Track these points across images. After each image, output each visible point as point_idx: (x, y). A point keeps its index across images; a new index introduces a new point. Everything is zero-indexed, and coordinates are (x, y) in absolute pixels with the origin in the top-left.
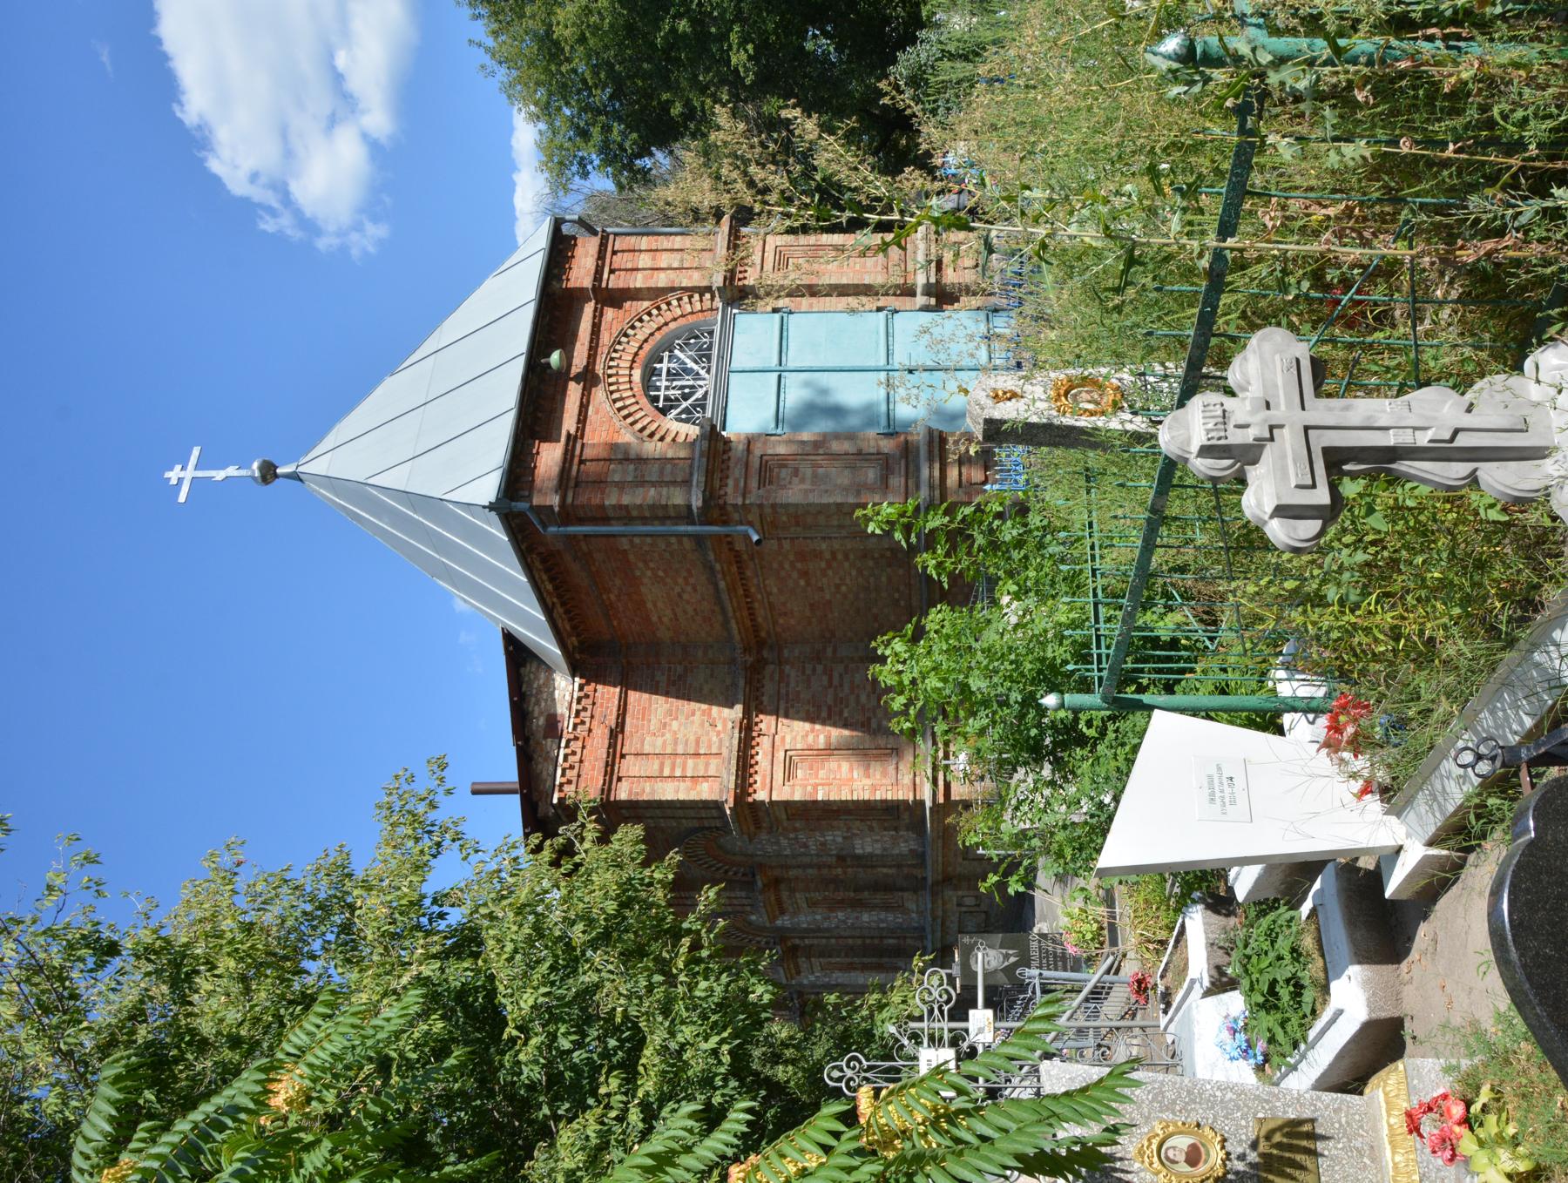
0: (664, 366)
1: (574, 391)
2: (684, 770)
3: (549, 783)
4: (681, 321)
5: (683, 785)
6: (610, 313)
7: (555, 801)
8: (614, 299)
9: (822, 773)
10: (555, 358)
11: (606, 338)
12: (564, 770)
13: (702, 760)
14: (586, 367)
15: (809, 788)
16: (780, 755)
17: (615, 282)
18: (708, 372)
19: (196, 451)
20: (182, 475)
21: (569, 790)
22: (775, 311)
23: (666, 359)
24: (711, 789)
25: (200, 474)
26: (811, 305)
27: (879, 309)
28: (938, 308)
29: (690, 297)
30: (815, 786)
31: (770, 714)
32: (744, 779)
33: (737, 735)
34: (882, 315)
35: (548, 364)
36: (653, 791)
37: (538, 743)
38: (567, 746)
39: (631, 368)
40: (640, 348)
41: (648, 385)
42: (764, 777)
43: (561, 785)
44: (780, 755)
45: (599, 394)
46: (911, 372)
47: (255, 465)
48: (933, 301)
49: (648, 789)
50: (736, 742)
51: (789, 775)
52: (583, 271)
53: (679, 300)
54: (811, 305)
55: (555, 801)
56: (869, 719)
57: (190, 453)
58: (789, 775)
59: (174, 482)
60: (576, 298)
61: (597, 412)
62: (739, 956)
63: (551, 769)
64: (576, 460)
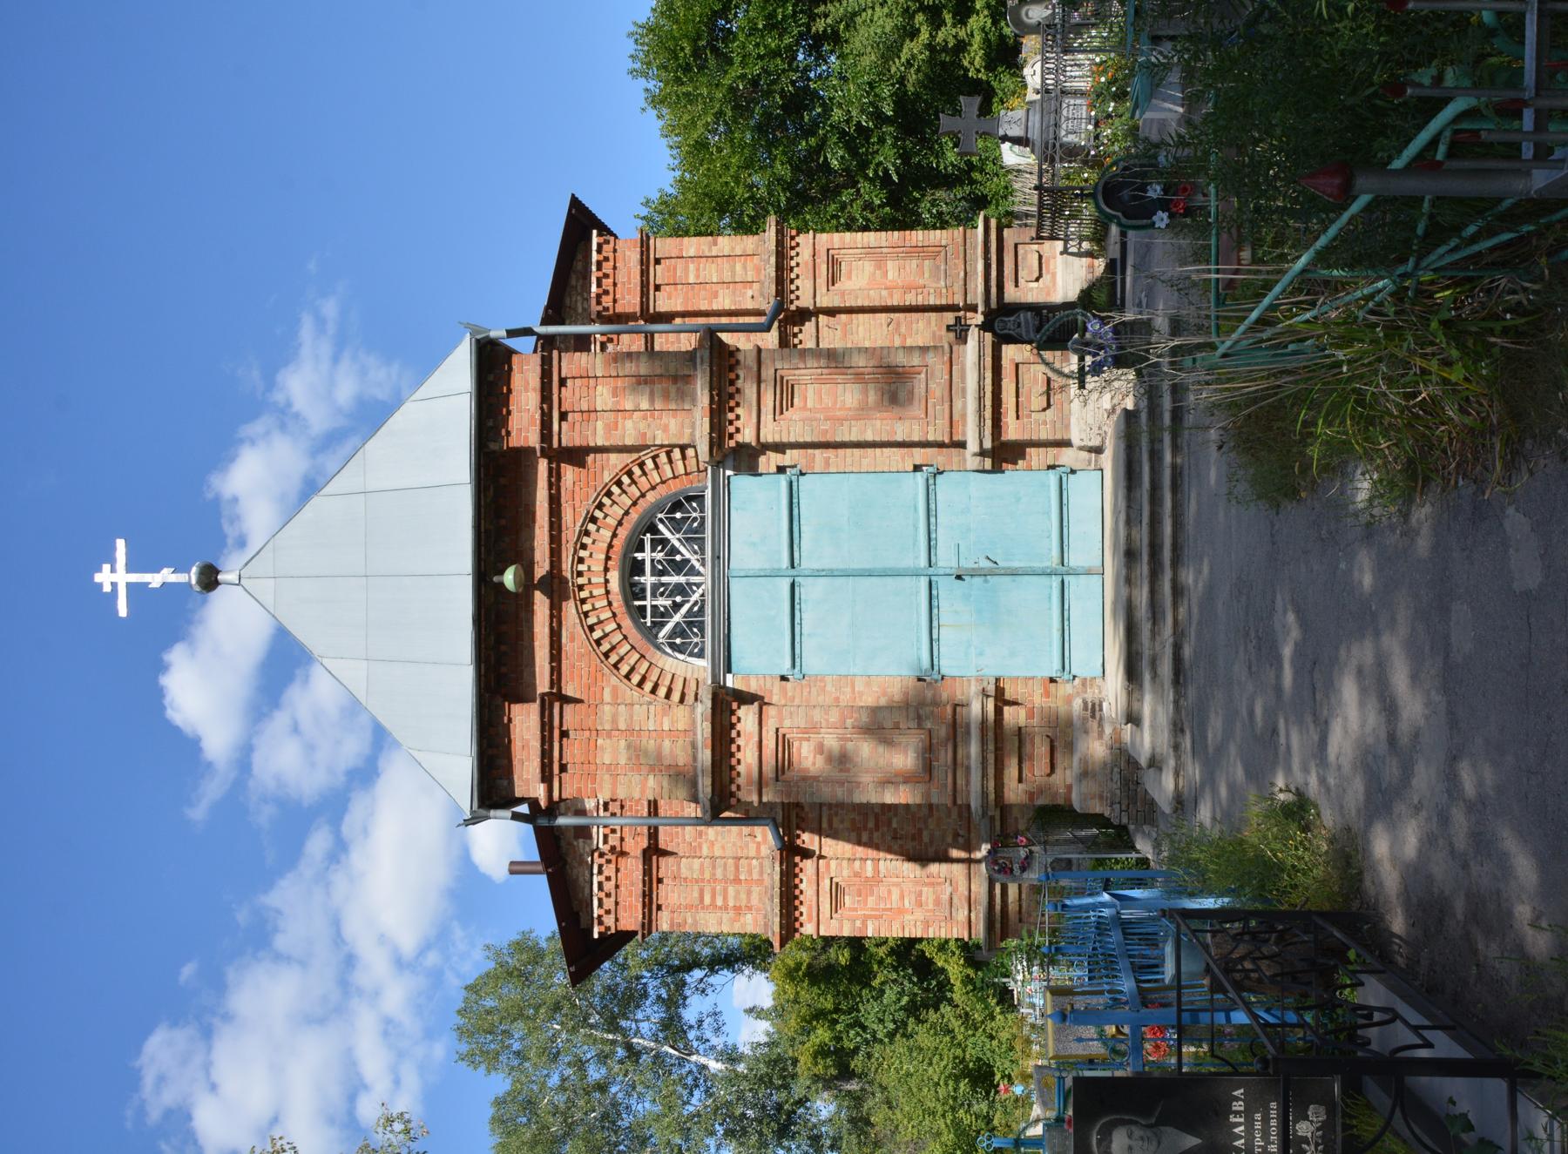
0: (646, 556)
1: (541, 603)
2: (725, 898)
3: (587, 891)
4: (662, 490)
5: (725, 917)
6: (569, 473)
7: (596, 936)
8: (577, 456)
9: (871, 901)
10: (509, 578)
11: (571, 520)
12: (600, 900)
13: (743, 888)
14: (550, 573)
15: (858, 923)
16: (825, 884)
17: (569, 435)
18: (703, 565)
19: (123, 611)
20: (114, 577)
21: (609, 921)
22: (781, 470)
23: (648, 546)
24: (755, 920)
25: (135, 578)
26: (827, 462)
27: (917, 468)
28: (997, 469)
29: (668, 454)
30: (865, 919)
31: (812, 831)
32: (788, 882)
33: (778, 869)
34: (920, 478)
35: (502, 584)
36: (695, 922)
37: (570, 844)
38: (600, 872)
39: (606, 570)
40: (614, 535)
41: (633, 592)
42: (810, 907)
43: (600, 917)
44: (825, 884)
45: (570, 609)
46: (959, 577)
47: (194, 569)
48: (988, 463)
49: (690, 921)
50: (777, 877)
51: (836, 904)
52: (525, 422)
53: (654, 458)
54: (827, 462)
55: (596, 936)
56: (920, 830)
57: (114, 549)
58: (836, 904)
59: (107, 588)
60: (523, 457)
61: (572, 640)
62: (840, 194)
63: (587, 873)
64: (556, 733)
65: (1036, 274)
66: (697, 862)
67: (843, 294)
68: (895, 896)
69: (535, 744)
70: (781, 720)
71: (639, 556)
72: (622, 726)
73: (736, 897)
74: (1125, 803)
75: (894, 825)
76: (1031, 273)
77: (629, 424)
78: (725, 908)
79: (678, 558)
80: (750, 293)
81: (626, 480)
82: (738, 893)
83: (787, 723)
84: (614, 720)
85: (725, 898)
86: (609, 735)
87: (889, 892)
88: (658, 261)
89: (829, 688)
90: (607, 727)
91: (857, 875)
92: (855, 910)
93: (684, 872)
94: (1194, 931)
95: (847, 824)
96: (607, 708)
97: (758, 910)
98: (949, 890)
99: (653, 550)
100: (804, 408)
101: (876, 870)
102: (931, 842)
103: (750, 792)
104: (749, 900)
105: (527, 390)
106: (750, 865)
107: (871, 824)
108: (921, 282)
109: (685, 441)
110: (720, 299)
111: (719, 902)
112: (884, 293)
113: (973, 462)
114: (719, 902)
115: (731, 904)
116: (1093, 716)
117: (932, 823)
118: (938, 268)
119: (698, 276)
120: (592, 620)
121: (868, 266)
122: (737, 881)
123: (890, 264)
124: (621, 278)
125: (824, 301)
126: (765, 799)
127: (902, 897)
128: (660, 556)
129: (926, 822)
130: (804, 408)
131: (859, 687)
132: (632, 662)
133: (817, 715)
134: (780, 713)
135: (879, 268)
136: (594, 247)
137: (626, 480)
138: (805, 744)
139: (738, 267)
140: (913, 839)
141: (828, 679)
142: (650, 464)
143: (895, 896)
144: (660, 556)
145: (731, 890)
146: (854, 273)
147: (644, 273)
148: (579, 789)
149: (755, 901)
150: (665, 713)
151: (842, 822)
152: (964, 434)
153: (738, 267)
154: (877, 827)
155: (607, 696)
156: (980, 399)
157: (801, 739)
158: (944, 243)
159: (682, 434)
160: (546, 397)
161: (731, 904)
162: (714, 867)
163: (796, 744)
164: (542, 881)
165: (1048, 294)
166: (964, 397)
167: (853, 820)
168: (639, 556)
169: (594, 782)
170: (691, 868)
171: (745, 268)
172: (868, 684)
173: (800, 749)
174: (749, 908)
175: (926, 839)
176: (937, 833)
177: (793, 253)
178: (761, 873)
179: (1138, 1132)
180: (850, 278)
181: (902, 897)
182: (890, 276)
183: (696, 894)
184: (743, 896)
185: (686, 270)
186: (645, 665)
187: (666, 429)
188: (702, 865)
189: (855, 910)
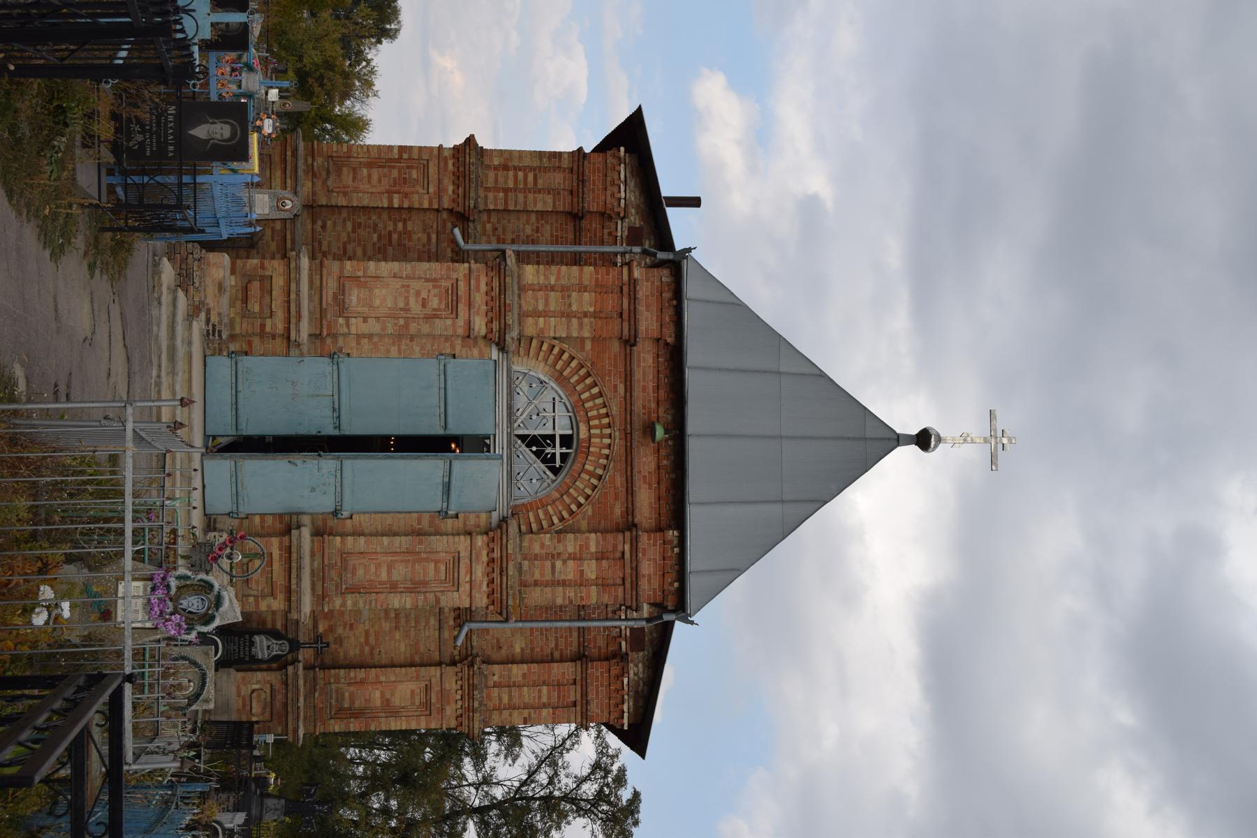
2: (516, 177)
7: (622, 149)
55: (622, 149)
56: (354, 232)
65: (254, 695)
66: (539, 207)
67: (418, 678)
68: (375, 177)
69: (641, 308)
70: (454, 324)
71: (564, 450)
72: (575, 321)
73: (507, 179)
74: (190, 261)
75: (375, 236)
76: (259, 696)
77: (570, 549)
78: (516, 169)
79: (534, 449)
80: (496, 678)
81: (574, 507)
82: (506, 182)
83: (449, 322)
84: (581, 325)
85: (516, 177)
86: (585, 314)
87: (380, 181)
88: (575, 704)
89: (417, 349)
90: (586, 320)
91: (406, 195)
92: (408, 167)
93: (549, 199)
94: (186, 220)
95: (415, 237)
96: (586, 334)
97: (488, 167)
98: (329, 183)
99: (554, 454)
100: (436, 562)
101: (391, 200)
102: (344, 221)
103: (478, 270)
104: (496, 176)
105: (649, 575)
106: (496, 204)
107: (395, 236)
108: (352, 689)
109: (528, 537)
110: (520, 673)
111: (521, 174)
112: (383, 679)
113: (306, 520)
114: (521, 174)
115: (511, 173)
116: (214, 326)
117: (344, 237)
118: (337, 700)
119: (540, 691)
120: (599, 401)
121: (397, 701)
122: (506, 190)
123: (378, 703)
124: (603, 690)
125: (434, 672)
126: (466, 265)
127: (370, 176)
128: (549, 450)
129: (349, 236)
130: (436, 562)
131: (394, 350)
132: (568, 370)
133: (426, 329)
134: (455, 331)
135: (388, 700)
136: (626, 715)
137: (574, 507)
138: (435, 306)
139: (505, 700)
140: (360, 224)
141: (418, 356)
142: (555, 520)
143: (375, 177)
144: (549, 450)
145: (511, 184)
146: (409, 696)
147: (584, 694)
148: (608, 274)
149: (491, 174)
150: (542, 330)
151: (419, 239)
152: (313, 542)
153: (505, 700)
154: (390, 233)
155: (588, 345)
156: (299, 568)
157: (439, 310)
158: (332, 721)
159: (531, 541)
160: (636, 570)
161: (511, 173)
162: (525, 203)
163: (443, 306)
164: (666, 191)
165: (243, 678)
166: (312, 571)
167: (410, 240)
168: (564, 450)
169: (597, 279)
170: (545, 202)
171: (500, 699)
172: (388, 351)
173: (440, 302)
174: (496, 169)
175: (349, 225)
176: (339, 228)
177: (459, 712)
178: (486, 198)
179: (218, 136)
180: (413, 692)
181: (370, 176)
182: (378, 694)
183: (540, 181)
184: (501, 180)
185: (549, 697)
186: (558, 367)
187: (542, 545)
188: (535, 205)
189: (408, 167)
